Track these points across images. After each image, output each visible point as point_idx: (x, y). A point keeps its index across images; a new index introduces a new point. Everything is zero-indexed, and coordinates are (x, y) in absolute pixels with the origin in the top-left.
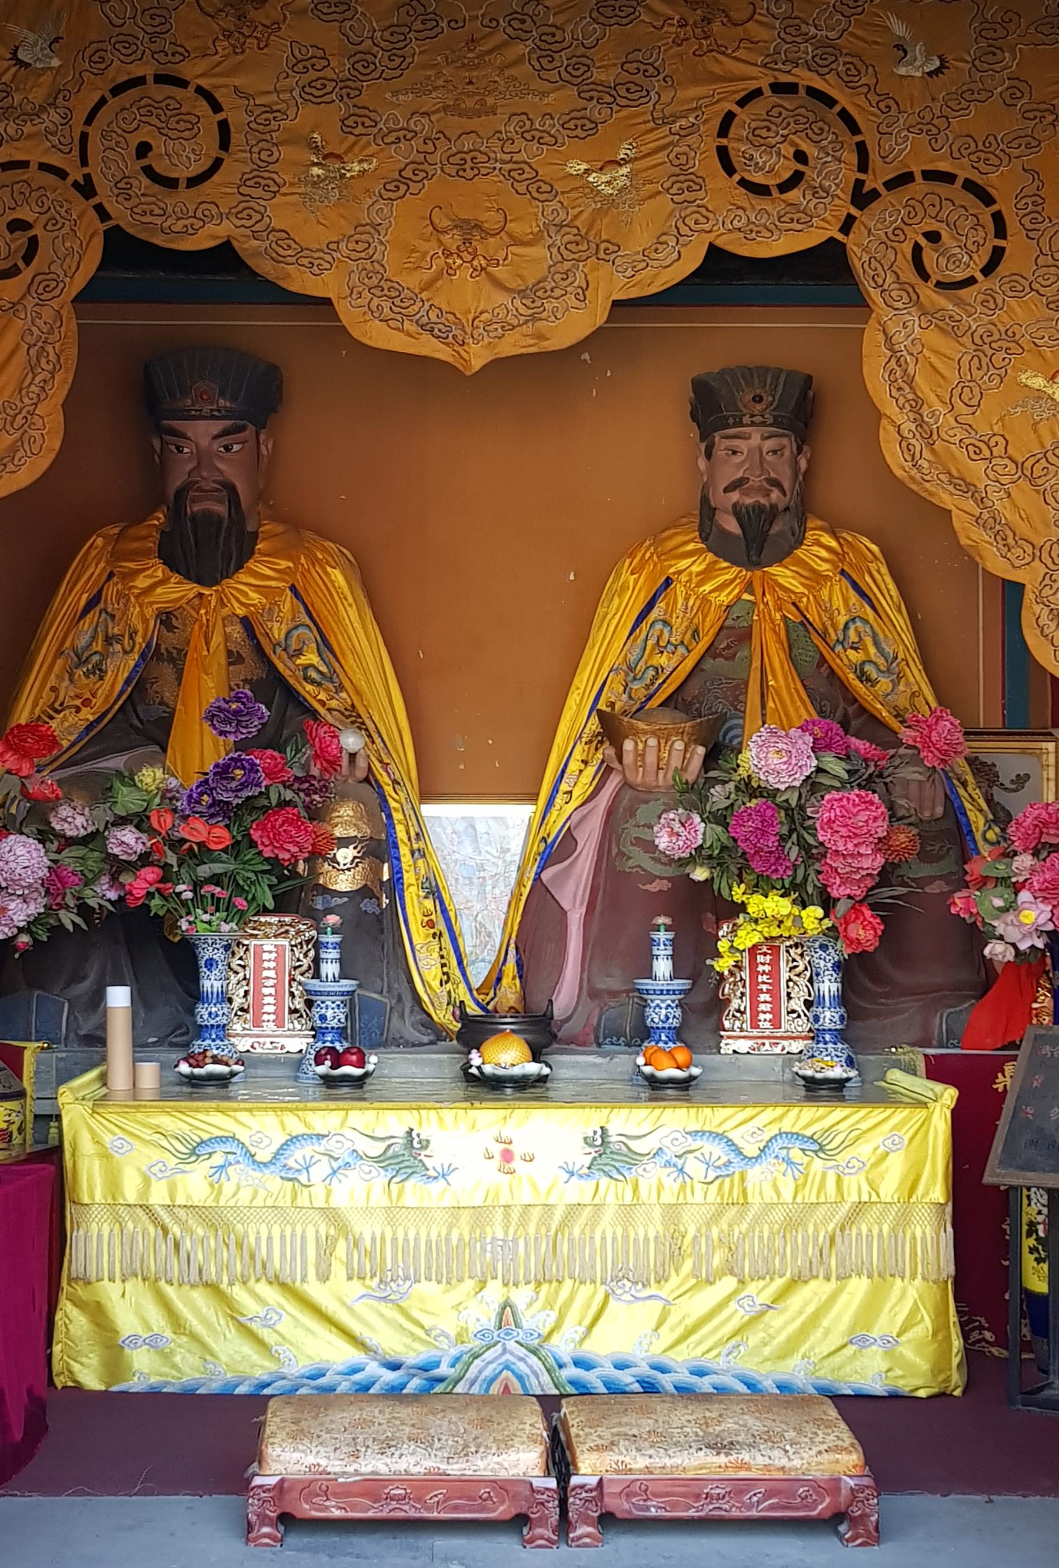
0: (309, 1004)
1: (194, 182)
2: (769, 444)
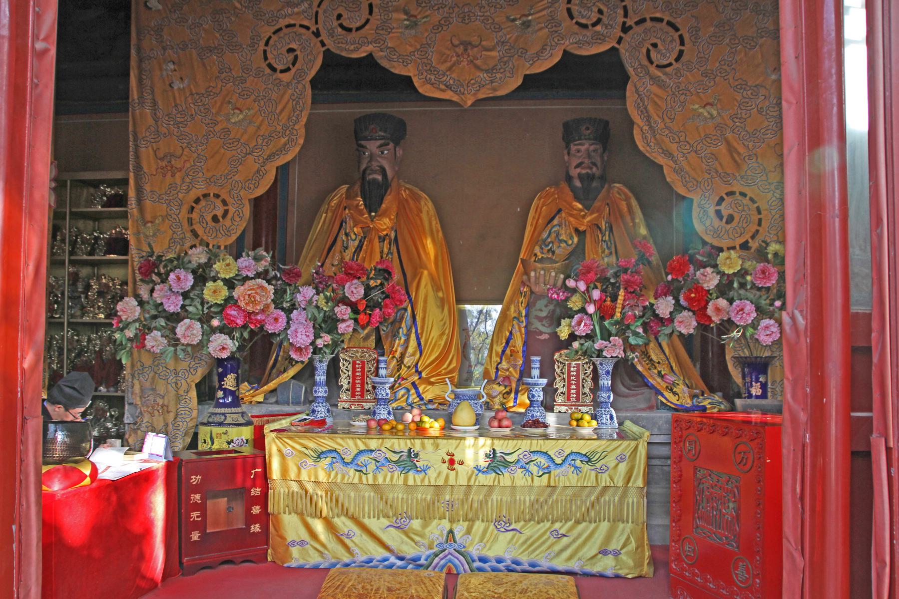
0: (374, 388)
1: (358, 29)
2: (592, 148)
